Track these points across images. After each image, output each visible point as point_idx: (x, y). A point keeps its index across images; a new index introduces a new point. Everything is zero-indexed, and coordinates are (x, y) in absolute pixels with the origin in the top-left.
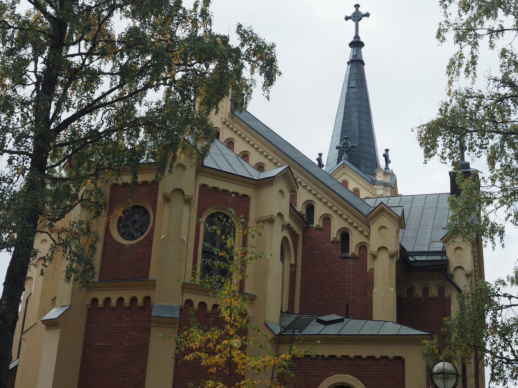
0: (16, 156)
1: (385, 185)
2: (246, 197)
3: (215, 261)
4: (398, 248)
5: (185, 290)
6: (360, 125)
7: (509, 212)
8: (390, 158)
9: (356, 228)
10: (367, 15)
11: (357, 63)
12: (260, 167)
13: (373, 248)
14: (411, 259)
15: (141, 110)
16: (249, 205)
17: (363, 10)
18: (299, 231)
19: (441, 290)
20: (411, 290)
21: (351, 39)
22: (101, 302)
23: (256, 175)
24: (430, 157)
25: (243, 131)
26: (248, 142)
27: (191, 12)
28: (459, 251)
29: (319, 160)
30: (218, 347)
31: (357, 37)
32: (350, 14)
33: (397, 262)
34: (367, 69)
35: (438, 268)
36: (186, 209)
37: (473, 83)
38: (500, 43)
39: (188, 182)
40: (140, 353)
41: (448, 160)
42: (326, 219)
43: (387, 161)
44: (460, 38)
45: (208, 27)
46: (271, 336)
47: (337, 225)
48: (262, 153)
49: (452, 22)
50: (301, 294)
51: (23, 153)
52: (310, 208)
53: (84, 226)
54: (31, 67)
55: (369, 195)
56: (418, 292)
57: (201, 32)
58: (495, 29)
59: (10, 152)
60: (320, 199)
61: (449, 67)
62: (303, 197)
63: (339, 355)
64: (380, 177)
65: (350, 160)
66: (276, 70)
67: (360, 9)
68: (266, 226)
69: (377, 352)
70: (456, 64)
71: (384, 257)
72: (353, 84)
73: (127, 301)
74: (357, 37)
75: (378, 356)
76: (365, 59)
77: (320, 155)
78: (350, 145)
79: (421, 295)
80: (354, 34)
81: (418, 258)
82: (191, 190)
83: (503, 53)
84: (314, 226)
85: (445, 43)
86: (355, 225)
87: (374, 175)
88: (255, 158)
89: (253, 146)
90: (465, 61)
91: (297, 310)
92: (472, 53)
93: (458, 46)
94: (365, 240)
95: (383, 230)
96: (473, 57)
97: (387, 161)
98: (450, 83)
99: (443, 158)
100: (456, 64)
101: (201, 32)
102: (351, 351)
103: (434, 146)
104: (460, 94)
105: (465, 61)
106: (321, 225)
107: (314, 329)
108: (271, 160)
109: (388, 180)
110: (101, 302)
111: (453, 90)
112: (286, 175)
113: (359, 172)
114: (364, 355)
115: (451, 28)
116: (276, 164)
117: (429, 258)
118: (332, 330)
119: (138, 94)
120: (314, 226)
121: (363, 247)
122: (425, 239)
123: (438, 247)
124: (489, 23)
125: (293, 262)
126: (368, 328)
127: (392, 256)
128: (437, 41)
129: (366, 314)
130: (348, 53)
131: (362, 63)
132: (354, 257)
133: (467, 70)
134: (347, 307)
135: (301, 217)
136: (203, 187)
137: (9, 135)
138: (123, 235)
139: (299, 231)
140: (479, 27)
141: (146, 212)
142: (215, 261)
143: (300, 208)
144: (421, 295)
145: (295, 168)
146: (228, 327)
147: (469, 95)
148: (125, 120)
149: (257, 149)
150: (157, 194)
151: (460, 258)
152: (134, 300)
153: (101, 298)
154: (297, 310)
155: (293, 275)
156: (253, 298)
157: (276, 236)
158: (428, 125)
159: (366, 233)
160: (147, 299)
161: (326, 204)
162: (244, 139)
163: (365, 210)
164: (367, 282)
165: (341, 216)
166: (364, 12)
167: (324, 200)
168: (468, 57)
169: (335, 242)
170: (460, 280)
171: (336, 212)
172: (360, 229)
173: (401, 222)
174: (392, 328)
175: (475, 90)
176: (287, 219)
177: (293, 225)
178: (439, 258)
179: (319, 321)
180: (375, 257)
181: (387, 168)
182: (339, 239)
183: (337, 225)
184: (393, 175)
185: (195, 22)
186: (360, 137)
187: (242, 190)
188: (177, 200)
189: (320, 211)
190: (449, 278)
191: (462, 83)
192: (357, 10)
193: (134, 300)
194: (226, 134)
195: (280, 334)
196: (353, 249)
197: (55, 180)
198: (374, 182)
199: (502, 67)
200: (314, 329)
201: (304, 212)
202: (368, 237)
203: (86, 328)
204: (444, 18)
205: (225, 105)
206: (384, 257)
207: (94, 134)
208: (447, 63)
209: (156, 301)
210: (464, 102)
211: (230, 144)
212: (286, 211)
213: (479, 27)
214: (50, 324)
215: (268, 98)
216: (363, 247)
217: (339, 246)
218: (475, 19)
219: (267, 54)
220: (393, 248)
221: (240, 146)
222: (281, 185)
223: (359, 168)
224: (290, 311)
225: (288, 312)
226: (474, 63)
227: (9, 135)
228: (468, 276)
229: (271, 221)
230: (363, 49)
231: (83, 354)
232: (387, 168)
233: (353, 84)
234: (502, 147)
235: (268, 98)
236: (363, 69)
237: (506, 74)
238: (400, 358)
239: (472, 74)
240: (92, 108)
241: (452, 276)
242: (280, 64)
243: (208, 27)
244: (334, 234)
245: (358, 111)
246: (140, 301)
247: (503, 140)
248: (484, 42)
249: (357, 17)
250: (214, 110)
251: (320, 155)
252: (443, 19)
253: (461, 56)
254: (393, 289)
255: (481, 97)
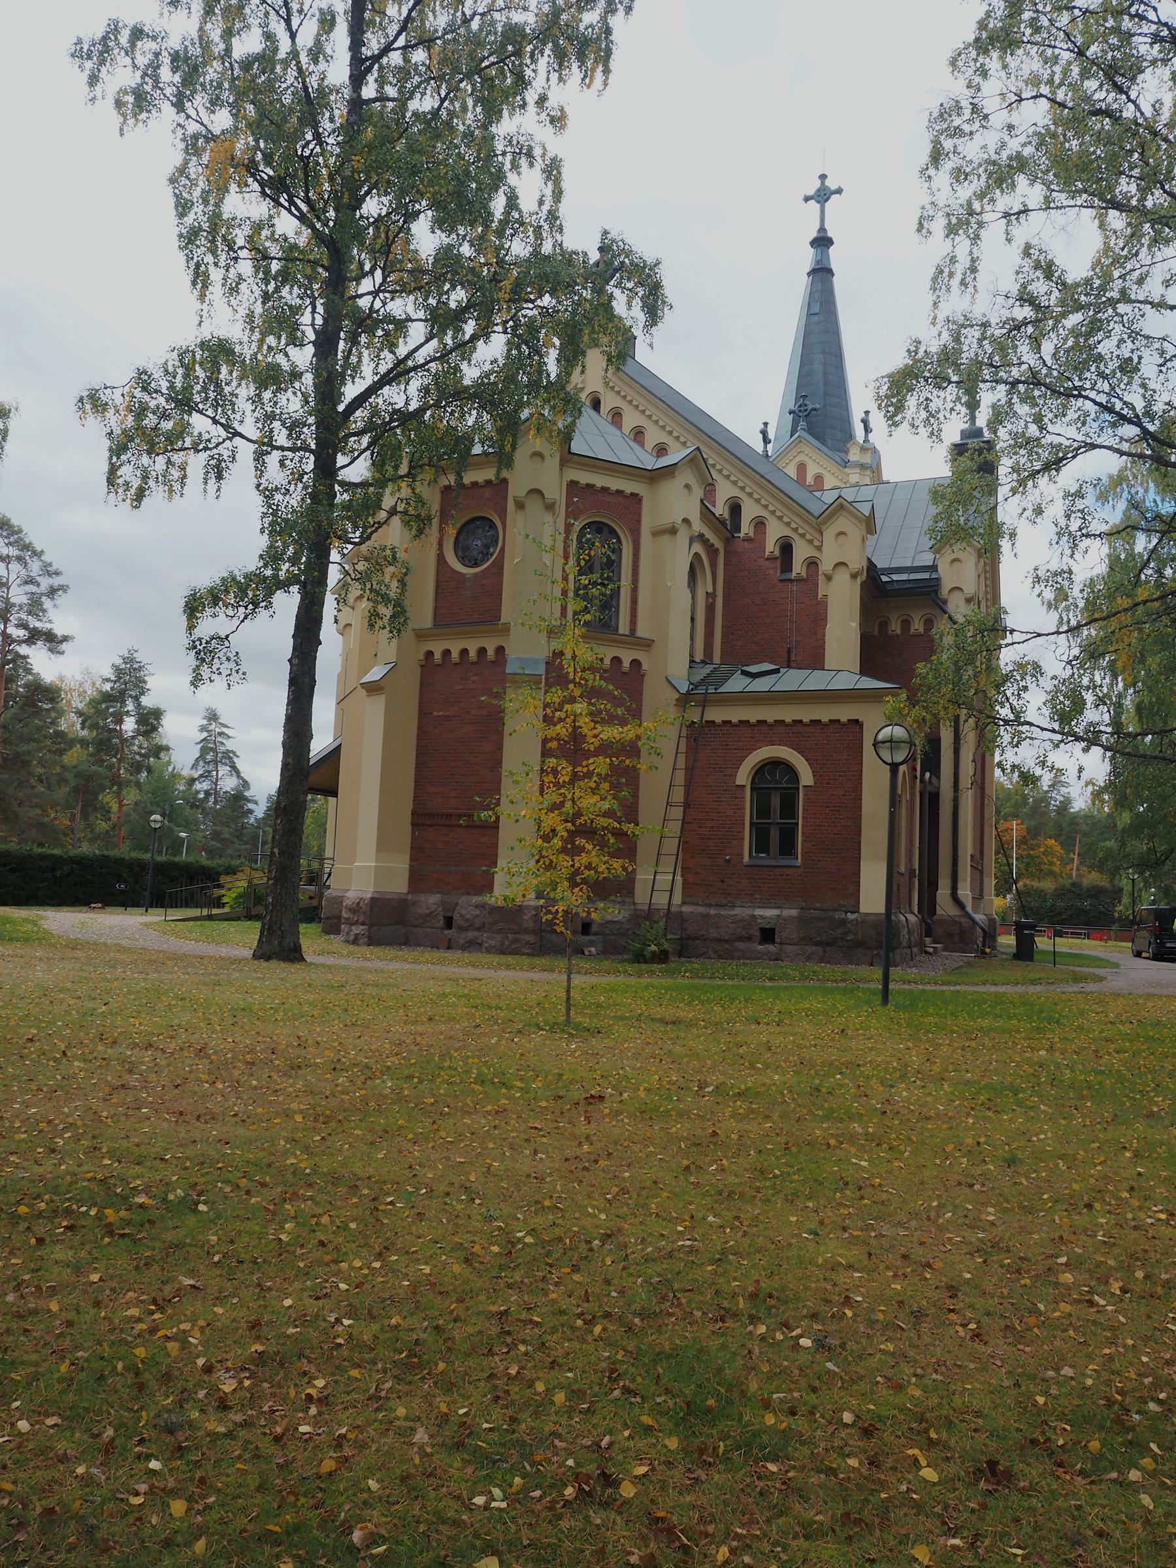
0: (289, 454)
1: (863, 467)
2: (636, 498)
3: (600, 593)
4: (865, 564)
5: (624, 628)
6: (825, 374)
7: (1024, 505)
8: (872, 425)
9: (803, 536)
10: (839, 191)
11: (822, 273)
12: (661, 450)
13: (826, 566)
14: (884, 579)
15: (470, 374)
16: (640, 509)
17: (831, 184)
18: (718, 543)
19: (929, 624)
20: (884, 625)
21: (814, 234)
22: (437, 656)
23: (650, 462)
24: (896, 425)
25: (636, 396)
26: (643, 412)
27: (531, 215)
28: (956, 564)
29: (764, 433)
30: (558, 714)
31: (822, 229)
32: (811, 193)
33: (863, 584)
34: (839, 283)
35: (925, 592)
36: (548, 517)
37: (972, 303)
38: (1023, 232)
39: (551, 479)
40: (492, 725)
41: (922, 430)
42: (760, 524)
43: (867, 430)
44: (952, 230)
45: (558, 237)
46: (677, 696)
47: (774, 532)
48: (663, 428)
49: (941, 204)
50: (724, 635)
51: (301, 449)
52: (735, 509)
53: (388, 552)
54: (306, 318)
55: (836, 482)
56: (895, 627)
57: (547, 248)
58: (1015, 210)
59: (282, 448)
60: (750, 495)
61: (934, 279)
62: (724, 492)
63: (770, 720)
64: (854, 455)
65: (811, 430)
66: (664, 302)
67: (828, 183)
68: (666, 538)
69: (825, 713)
70: (946, 274)
71: (842, 577)
72: (816, 309)
73: (473, 654)
74: (822, 229)
75: (825, 719)
76: (834, 266)
77: (766, 424)
78: (810, 407)
79: (899, 632)
80: (818, 226)
81: (895, 577)
82: (555, 491)
83: (1027, 251)
84: (742, 535)
85: (931, 239)
86: (801, 531)
87: (846, 452)
88: (653, 436)
89: (650, 417)
90: (959, 269)
91: (717, 658)
92: (971, 253)
93: (949, 242)
94: (815, 553)
95: (842, 537)
96: (973, 261)
97: (867, 430)
98: (935, 304)
99: (913, 426)
100: (946, 274)
101: (547, 248)
102: (788, 714)
103: (900, 407)
104: (954, 322)
105: (959, 269)
106: (751, 534)
107: (737, 684)
108: (677, 438)
109: (867, 459)
110: (437, 656)
111: (941, 317)
112: (696, 461)
113: (823, 448)
114: (806, 720)
115: (940, 213)
116: (684, 444)
117: (913, 576)
118: (762, 685)
119: (465, 348)
120: (742, 535)
121: (812, 564)
122: (904, 549)
123: (927, 559)
124: (1005, 201)
125: (710, 590)
126: (814, 681)
127: (854, 576)
128: (917, 238)
129: (816, 661)
130: (807, 258)
131: (830, 272)
132: (799, 580)
133: (963, 283)
134: (789, 652)
135: (722, 522)
136: (573, 484)
137: (276, 424)
138: (462, 560)
139: (718, 543)
140: (988, 208)
141: (492, 525)
142: (600, 593)
143: (721, 509)
144: (899, 632)
145: (709, 447)
146: (571, 686)
147: (967, 323)
148: (446, 390)
149: (656, 422)
150: (506, 498)
151: (959, 575)
152: (482, 651)
153: (437, 649)
154: (717, 658)
155: (710, 609)
156: (647, 644)
157: (680, 554)
158: (889, 376)
159: (816, 543)
160: (500, 650)
161: (758, 501)
162: (637, 407)
163: (816, 509)
164: (818, 616)
165: (780, 518)
166: (833, 187)
167: (756, 496)
168: (963, 261)
169: (771, 559)
170: (958, 608)
171: (773, 512)
172: (808, 537)
173: (869, 524)
174: (849, 679)
175: (977, 314)
176: (698, 526)
177: (709, 535)
178: (926, 576)
179: (744, 673)
180: (829, 578)
181: (866, 440)
182: (777, 553)
183: (774, 532)
184: (875, 450)
185: (538, 230)
186: (826, 394)
187: (629, 487)
188: (534, 507)
189: (749, 512)
190: (940, 605)
191: (955, 303)
192: (823, 183)
193: (482, 651)
194: (609, 402)
195: (688, 693)
196: (798, 568)
197: (347, 486)
198: (845, 464)
199: (1018, 273)
200: (737, 684)
201: (726, 515)
202: (819, 548)
203: (421, 691)
204: (929, 199)
205: (595, 360)
206: (842, 577)
207: (404, 417)
208: (932, 271)
209: (512, 654)
210: (959, 334)
211: (616, 416)
212: (695, 515)
213: (988, 208)
214: (373, 688)
215: (651, 346)
216: (812, 564)
217: (778, 563)
218: (981, 196)
219: (649, 276)
220: (857, 563)
221: (631, 419)
222: (687, 476)
223: (824, 443)
224: (707, 660)
225: (703, 662)
226: (973, 270)
227: (276, 424)
228: (968, 601)
229: (673, 531)
230: (832, 250)
231: (419, 728)
232: (866, 440)
233: (816, 309)
234: (1010, 403)
235: (651, 346)
236: (831, 283)
237: (1024, 286)
238: (857, 721)
239: (971, 289)
240: (398, 373)
241: (945, 602)
242: (670, 290)
243: (558, 237)
244: (771, 546)
245: (824, 353)
246: (491, 653)
247: (1009, 393)
248: (994, 231)
249: (823, 195)
250: (579, 368)
251: (766, 424)
252: (926, 200)
253: (953, 260)
254: (855, 624)
255: (985, 325)
